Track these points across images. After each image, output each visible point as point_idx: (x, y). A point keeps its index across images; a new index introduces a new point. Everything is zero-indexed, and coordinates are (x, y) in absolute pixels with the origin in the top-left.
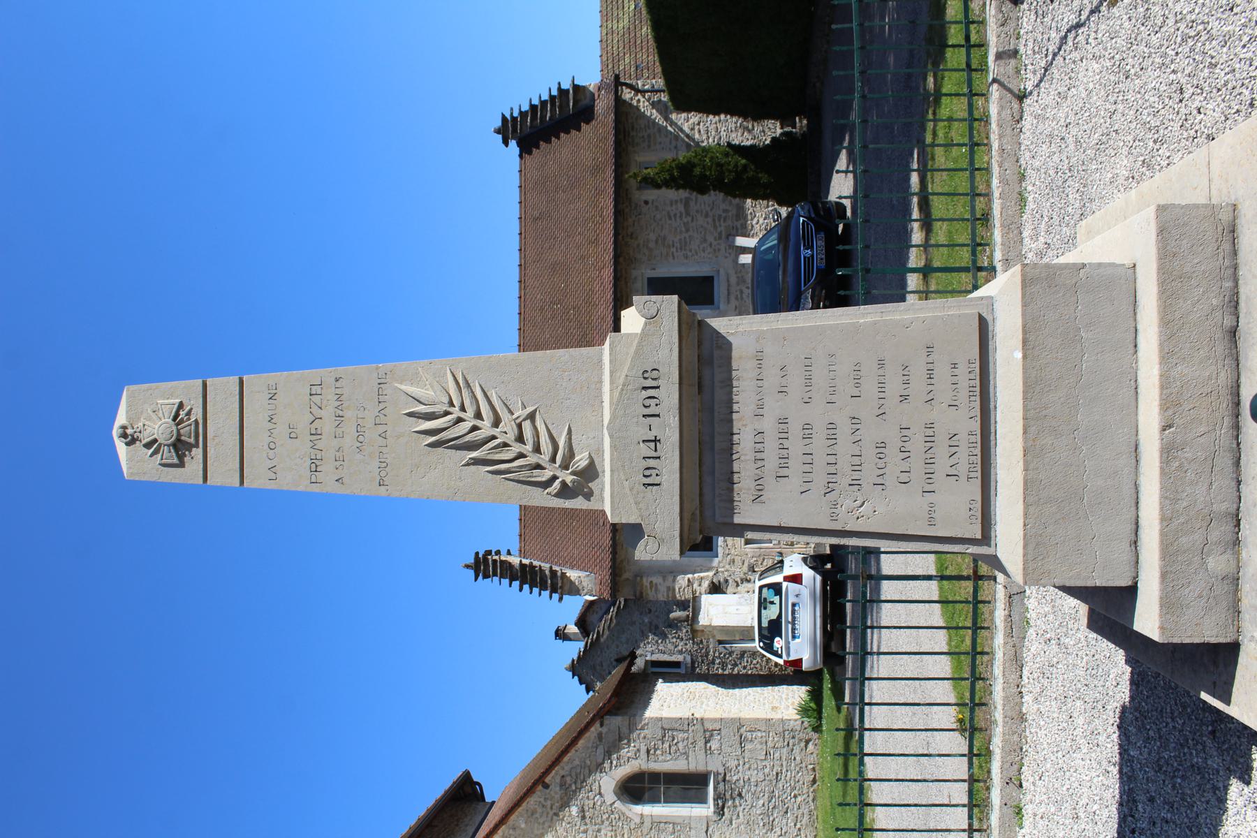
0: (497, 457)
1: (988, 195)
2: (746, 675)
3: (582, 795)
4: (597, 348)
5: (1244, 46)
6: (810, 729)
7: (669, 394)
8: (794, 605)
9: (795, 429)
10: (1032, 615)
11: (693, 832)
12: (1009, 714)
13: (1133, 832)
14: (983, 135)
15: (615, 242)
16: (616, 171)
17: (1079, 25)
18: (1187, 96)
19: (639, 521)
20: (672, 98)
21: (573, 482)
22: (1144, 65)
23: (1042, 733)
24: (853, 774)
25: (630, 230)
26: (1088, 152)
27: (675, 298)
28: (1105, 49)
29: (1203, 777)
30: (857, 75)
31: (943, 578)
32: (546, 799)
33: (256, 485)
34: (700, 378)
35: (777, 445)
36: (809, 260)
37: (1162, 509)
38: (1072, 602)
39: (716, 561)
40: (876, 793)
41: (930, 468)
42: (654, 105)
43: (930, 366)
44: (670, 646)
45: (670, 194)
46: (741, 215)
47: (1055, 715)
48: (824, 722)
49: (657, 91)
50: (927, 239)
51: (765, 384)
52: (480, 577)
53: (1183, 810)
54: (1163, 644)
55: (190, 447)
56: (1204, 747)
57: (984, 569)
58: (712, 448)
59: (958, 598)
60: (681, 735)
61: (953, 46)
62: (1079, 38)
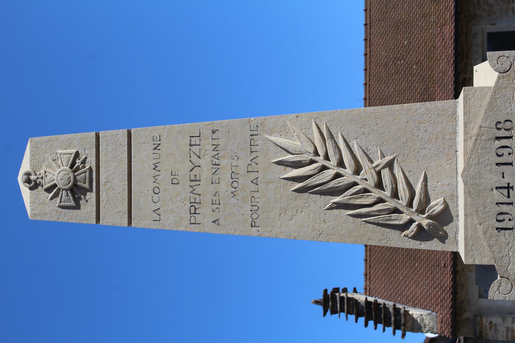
0: (358, 202)
19: (492, 262)
21: (429, 225)
33: (141, 225)
52: (329, 313)
55: (85, 191)
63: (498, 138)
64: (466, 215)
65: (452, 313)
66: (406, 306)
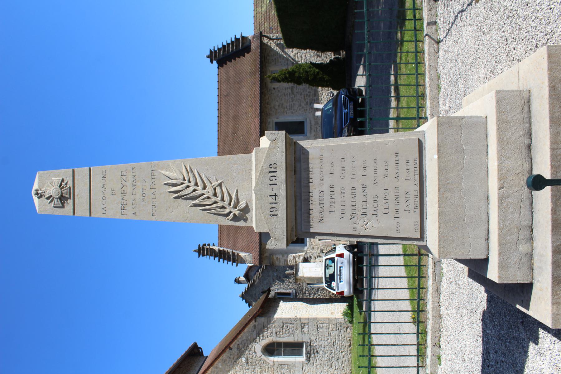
0: (205, 203)
1: (424, 86)
2: (320, 299)
3: (247, 352)
5: (533, 21)
6: (348, 322)
7: (281, 175)
8: (340, 267)
9: (337, 190)
10: (444, 271)
11: (296, 369)
12: (435, 315)
13: (488, 366)
14: (422, 59)
15: (261, 106)
16: (261, 74)
17: (463, 11)
18: (509, 42)
20: (286, 42)
21: (239, 214)
22: (491, 28)
23: (449, 323)
24: (367, 343)
25: (267, 101)
26: (467, 67)
27: (284, 132)
28: (474, 22)
29: (518, 342)
30: (366, 32)
31: (405, 255)
32: (231, 355)
33: (96, 216)
34: (295, 167)
35: (329, 197)
36: (346, 114)
37: (499, 224)
38: (462, 265)
39: (306, 248)
40: (377, 351)
41: (397, 207)
42: (277, 45)
43: (397, 162)
44: (286, 286)
45: (285, 85)
46: (316, 94)
47: (455, 315)
48: (354, 319)
49: (279, 39)
50: (398, 104)
51: (324, 170)
52: (201, 256)
53: (510, 356)
54: (500, 284)
55: (67, 199)
56: (519, 329)
57: (423, 252)
58: (301, 199)
59: (412, 264)
60: (291, 326)
61: (409, 20)
62: (463, 16)
63: (270, 172)
64: (256, 209)
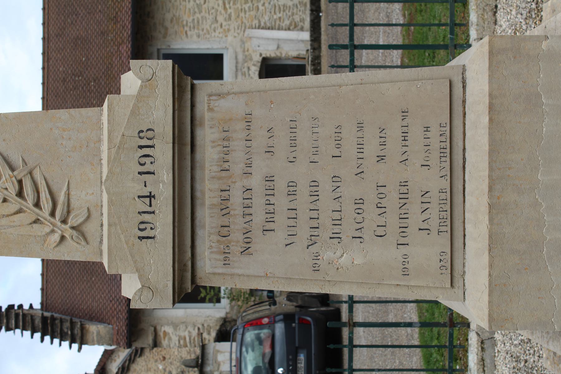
4: (97, 109)
9: (281, 185)
27: (171, 61)
35: (263, 201)
41: (404, 223)
51: (254, 144)
63: (141, 147)
65: (127, 325)
66: (83, 320)
